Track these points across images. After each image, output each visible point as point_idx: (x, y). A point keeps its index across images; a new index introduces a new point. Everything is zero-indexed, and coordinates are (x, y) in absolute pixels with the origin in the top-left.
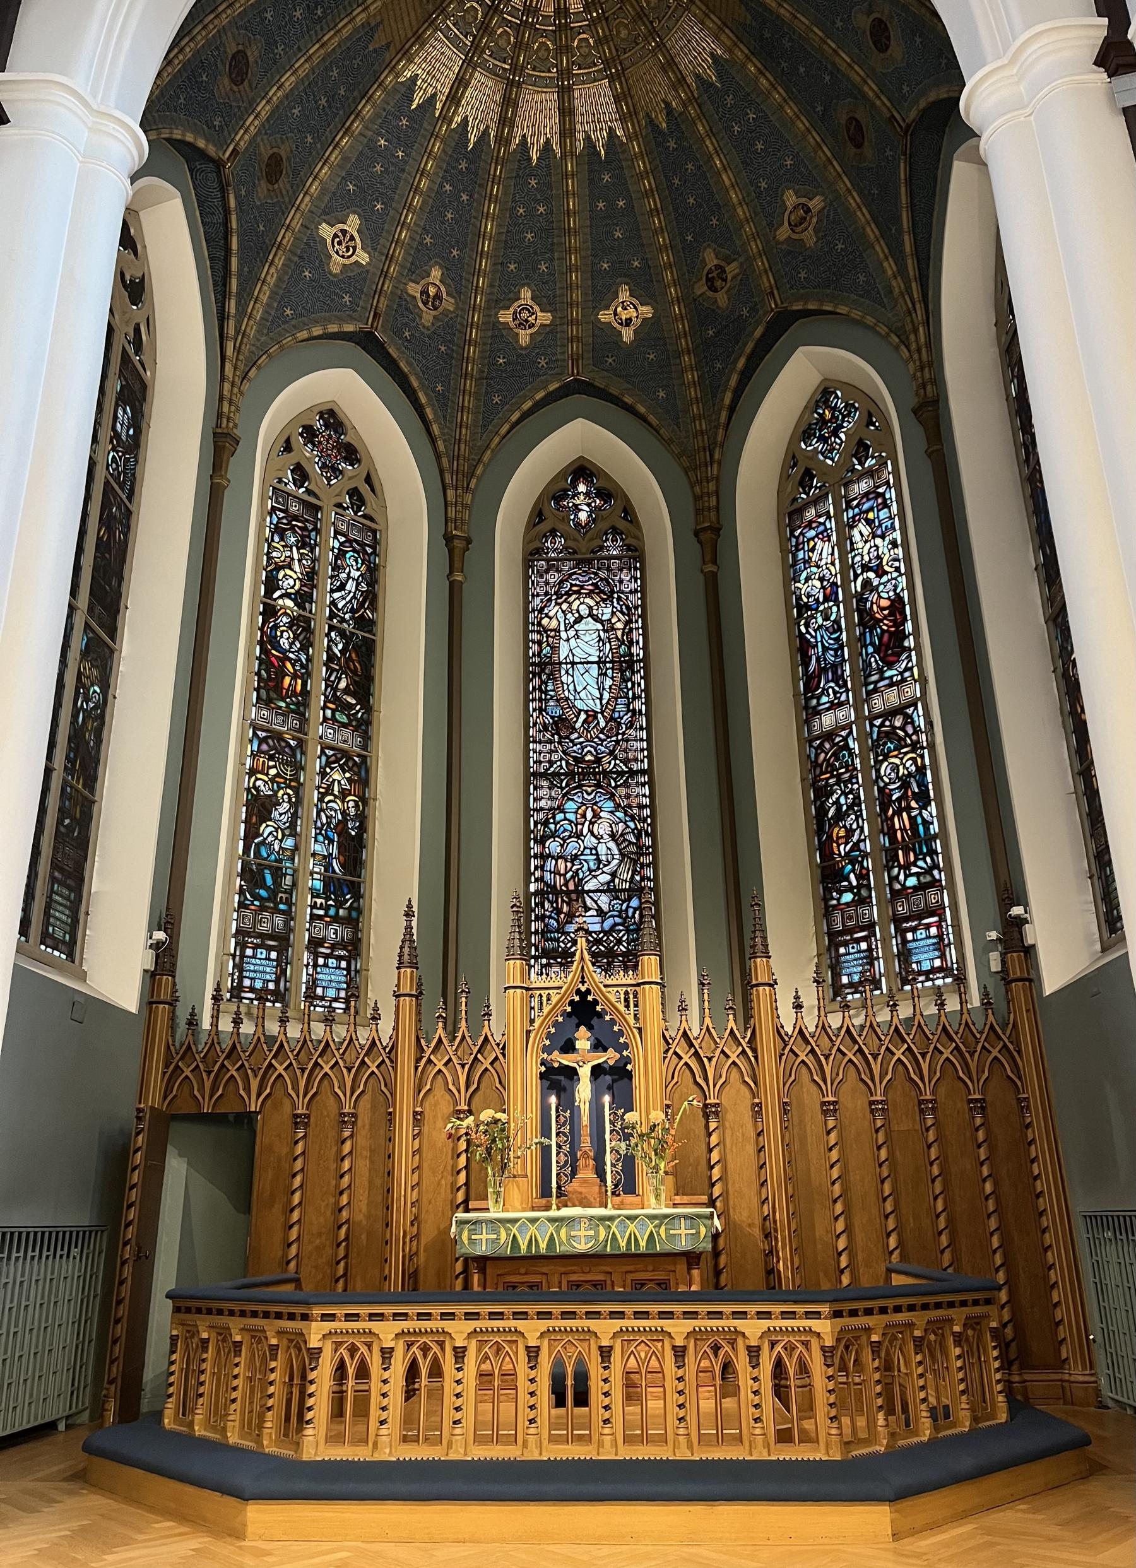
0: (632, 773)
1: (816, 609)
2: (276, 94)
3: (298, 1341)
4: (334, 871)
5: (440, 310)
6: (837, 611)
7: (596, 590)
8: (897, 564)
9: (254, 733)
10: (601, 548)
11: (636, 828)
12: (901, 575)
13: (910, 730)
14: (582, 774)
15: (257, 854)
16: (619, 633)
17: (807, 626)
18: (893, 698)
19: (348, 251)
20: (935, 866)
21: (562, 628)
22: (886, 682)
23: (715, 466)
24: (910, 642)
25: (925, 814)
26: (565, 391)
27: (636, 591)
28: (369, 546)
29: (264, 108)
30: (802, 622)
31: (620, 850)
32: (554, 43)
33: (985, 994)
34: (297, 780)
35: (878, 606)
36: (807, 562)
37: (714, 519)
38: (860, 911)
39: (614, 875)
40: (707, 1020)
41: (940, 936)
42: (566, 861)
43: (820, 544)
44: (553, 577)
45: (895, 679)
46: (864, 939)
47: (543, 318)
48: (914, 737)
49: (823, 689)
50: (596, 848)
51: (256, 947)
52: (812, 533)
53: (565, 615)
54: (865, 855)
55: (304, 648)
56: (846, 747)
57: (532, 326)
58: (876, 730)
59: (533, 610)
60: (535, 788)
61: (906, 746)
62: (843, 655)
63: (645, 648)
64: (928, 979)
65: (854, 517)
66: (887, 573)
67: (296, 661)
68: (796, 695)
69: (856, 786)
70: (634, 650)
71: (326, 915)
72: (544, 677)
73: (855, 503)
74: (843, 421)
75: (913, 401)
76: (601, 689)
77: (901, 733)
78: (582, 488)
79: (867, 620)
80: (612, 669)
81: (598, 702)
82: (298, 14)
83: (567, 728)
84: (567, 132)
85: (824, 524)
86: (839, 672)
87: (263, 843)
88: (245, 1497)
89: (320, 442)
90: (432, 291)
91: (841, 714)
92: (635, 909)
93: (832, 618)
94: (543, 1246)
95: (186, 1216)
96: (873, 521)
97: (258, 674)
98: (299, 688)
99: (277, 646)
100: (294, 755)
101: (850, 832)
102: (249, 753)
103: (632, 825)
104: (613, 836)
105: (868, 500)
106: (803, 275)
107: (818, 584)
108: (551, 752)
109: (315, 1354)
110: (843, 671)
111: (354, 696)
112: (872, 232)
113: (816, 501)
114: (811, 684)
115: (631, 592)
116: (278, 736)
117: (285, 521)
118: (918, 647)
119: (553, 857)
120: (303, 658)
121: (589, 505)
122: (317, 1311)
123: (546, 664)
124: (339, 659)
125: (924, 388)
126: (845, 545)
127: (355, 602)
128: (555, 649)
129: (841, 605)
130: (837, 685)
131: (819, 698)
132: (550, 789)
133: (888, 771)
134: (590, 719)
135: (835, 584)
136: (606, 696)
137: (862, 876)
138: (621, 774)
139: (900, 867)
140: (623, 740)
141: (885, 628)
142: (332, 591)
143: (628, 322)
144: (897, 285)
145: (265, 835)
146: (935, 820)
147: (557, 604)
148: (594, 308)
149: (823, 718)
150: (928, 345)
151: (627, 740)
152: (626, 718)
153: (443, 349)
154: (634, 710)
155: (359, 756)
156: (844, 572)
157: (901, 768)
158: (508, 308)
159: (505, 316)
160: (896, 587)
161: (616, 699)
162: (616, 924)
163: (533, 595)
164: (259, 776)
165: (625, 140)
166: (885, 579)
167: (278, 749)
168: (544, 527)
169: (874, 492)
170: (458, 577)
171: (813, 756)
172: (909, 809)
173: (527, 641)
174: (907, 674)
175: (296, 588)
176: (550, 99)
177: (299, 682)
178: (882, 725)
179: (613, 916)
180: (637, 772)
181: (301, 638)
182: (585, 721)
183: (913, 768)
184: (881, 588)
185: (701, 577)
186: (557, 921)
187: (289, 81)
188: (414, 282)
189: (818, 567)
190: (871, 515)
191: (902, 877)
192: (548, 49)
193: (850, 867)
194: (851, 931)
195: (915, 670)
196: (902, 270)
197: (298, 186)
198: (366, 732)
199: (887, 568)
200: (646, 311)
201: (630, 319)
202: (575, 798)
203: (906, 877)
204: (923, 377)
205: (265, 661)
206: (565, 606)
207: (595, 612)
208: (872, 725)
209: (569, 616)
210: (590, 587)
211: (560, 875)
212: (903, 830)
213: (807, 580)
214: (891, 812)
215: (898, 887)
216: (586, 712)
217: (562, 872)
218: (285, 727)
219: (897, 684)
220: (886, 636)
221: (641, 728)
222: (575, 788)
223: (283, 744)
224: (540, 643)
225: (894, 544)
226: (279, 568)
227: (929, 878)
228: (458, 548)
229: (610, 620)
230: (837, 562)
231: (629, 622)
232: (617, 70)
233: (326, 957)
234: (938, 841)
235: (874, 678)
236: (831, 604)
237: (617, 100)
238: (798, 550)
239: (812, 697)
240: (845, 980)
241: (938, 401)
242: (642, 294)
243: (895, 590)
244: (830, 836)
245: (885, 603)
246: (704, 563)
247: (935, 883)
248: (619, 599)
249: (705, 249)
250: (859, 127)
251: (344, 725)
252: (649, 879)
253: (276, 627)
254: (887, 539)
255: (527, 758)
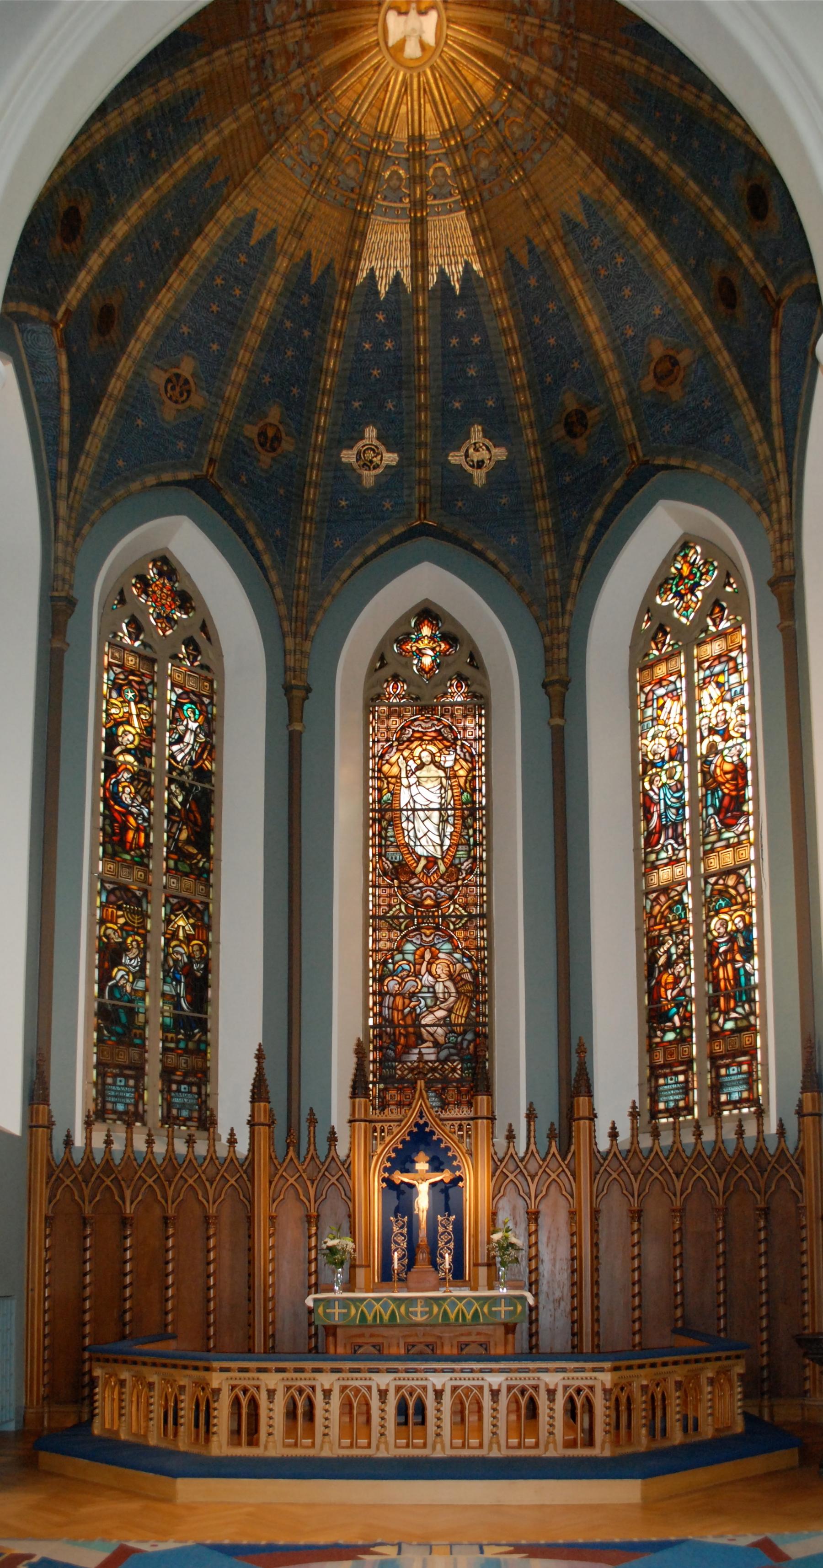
0: (471, 917)
1: (661, 767)
2: (107, 245)
3: (203, 1386)
4: (182, 1009)
5: (279, 451)
6: (682, 772)
7: (439, 737)
8: (742, 730)
9: (102, 885)
10: (445, 694)
11: (473, 968)
12: (746, 741)
13: (741, 889)
14: (423, 919)
15: (112, 996)
16: (462, 781)
17: (651, 782)
18: (728, 858)
19: (181, 395)
20: (752, 1013)
21: (403, 774)
22: (723, 843)
23: (567, 617)
24: (749, 807)
25: (748, 966)
26: (412, 534)
27: (480, 738)
28: (206, 699)
29: (95, 262)
30: (647, 779)
31: (457, 989)
32: (407, 171)
33: (781, 1125)
34: (144, 927)
35: (722, 770)
36: (655, 719)
37: (563, 672)
38: (680, 1049)
39: (450, 1011)
40: (532, 1147)
41: (750, 1073)
42: (404, 998)
43: (669, 703)
44: (395, 723)
45: (731, 841)
46: (681, 1072)
47: (390, 458)
48: (745, 897)
49: (663, 845)
50: (433, 987)
51: (115, 1076)
52: (661, 691)
53: (407, 762)
54: (690, 1000)
55: (146, 802)
56: (681, 901)
57: (377, 467)
58: (709, 887)
59: (374, 757)
60: (374, 931)
61: (737, 904)
62: (684, 815)
63: (488, 796)
64: (735, 1108)
65: (704, 679)
66: (732, 738)
67: (138, 815)
68: (636, 849)
69: (687, 938)
70: (477, 797)
71: (177, 1048)
72: (384, 823)
73: (707, 664)
74: (701, 579)
75: (770, 573)
76: (442, 836)
77: (733, 892)
78: (426, 631)
79: (711, 783)
80: (454, 816)
81: (438, 848)
82: (131, 160)
83: (406, 873)
84: (419, 266)
85: (674, 683)
86: (679, 830)
87: (116, 985)
88: (175, 1475)
89: (154, 592)
90: (271, 433)
91: (678, 870)
92: (470, 1042)
93: (676, 778)
94: (386, 1318)
95: (131, 1296)
96: (723, 684)
97: (103, 829)
98: (142, 840)
99: (119, 801)
100: (139, 904)
101: (677, 979)
102: (98, 904)
103: (469, 965)
104: (451, 977)
105: (720, 663)
106: (667, 428)
107: (664, 742)
108: (390, 896)
109: (217, 1392)
110: (683, 830)
111: (195, 845)
112: (741, 393)
113: (667, 658)
114: (651, 839)
115: (475, 740)
116: (125, 888)
117: (122, 676)
118: (756, 812)
119: (391, 995)
120: (145, 811)
121: (433, 649)
122: (216, 1365)
123: (387, 810)
124: (179, 811)
125: (782, 561)
126: (692, 705)
127: (193, 754)
128: (395, 795)
129: (686, 766)
130: (677, 842)
131: (658, 853)
132: (389, 931)
133: (718, 926)
134: (431, 864)
135: (680, 744)
136: (447, 842)
137: (686, 1018)
138: (461, 917)
139: (720, 1012)
140: (463, 885)
141: (726, 791)
142: (171, 744)
143: (480, 464)
144: (763, 450)
145: (118, 977)
146: (756, 973)
147: (398, 750)
148: (444, 449)
149: (661, 873)
150: (790, 516)
151: (467, 886)
152: (466, 865)
153: (282, 492)
154: (475, 858)
155: (202, 903)
156: (692, 729)
157: (730, 924)
158: (351, 448)
159: (348, 456)
160: (740, 752)
161: (457, 845)
162: (451, 1055)
163: (374, 741)
164: (109, 925)
165: (482, 275)
166: (730, 743)
167: (121, 897)
168: (387, 672)
169: (726, 655)
170: (297, 727)
171: (648, 907)
172: (734, 961)
173: (366, 787)
174: (743, 837)
175: (136, 743)
176: (402, 234)
177: (143, 835)
178: (716, 883)
179: (448, 1048)
180: (476, 916)
181: (143, 791)
182: (425, 867)
183: (741, 925)
184: (726, 752)
185: (548, 732)
186: (394, 1051)
187: (121, 229)
188: (249, 423)
189: (666, 726)
190: (721, 679)
191: (721, 1021)
192: (400, 178)
193: (674, 1010)
194: (671, 1066)
195: (752, 834)
196: (768, 436)
197: (130, 331)
198: (208, 880)
199: (732, 733)
200: (500, 453)
201: (483, 461)
202: (414, 940)
203: (725, 1021)
204: (781, 549)
205: (109, 815)
206: (406, 753)
207: (437, 759)
208: (706, 883)
209: (411, 763)
210: (433, 734)
211: (398, 1011)
212: (727, 979)
213: (654, 737)
214: (716, 963)
215: (716, 1029)
216: (427, 858)
217: (400, 1007)
218: (132, 879)
219: (733, 846)
220: (727, 799)
221: (482, 874)
222: (414, 930)
223: (130, 895)
224: (380, 790)
225: (742, 710)
226: (118, 724)
227: (744, 1023)
228: (296, 697)
229: (452, 767)
230: (685, 723)
231: (474, 769)
232: (476, 202)
233: (179, 1083)
234: (757, 992)
235: (713, 838)
236: (676, 763)
237: (475, 233)
238: (646, 706)
239: (652, 852)
240: (662, 1106)
241: (794, 576)
242: (494, 435)
243: (739, 755)
244: (659, 983)
245: (728, 767)
246: (552, 717)
247: (751, 1028)
248: (463, 746)
249: (565, 392)
250: (732, 289)
251: (187, 875)
252: (484, 1015)
253: (118, 783)
254: (735, 704)
255: (366, 902)
